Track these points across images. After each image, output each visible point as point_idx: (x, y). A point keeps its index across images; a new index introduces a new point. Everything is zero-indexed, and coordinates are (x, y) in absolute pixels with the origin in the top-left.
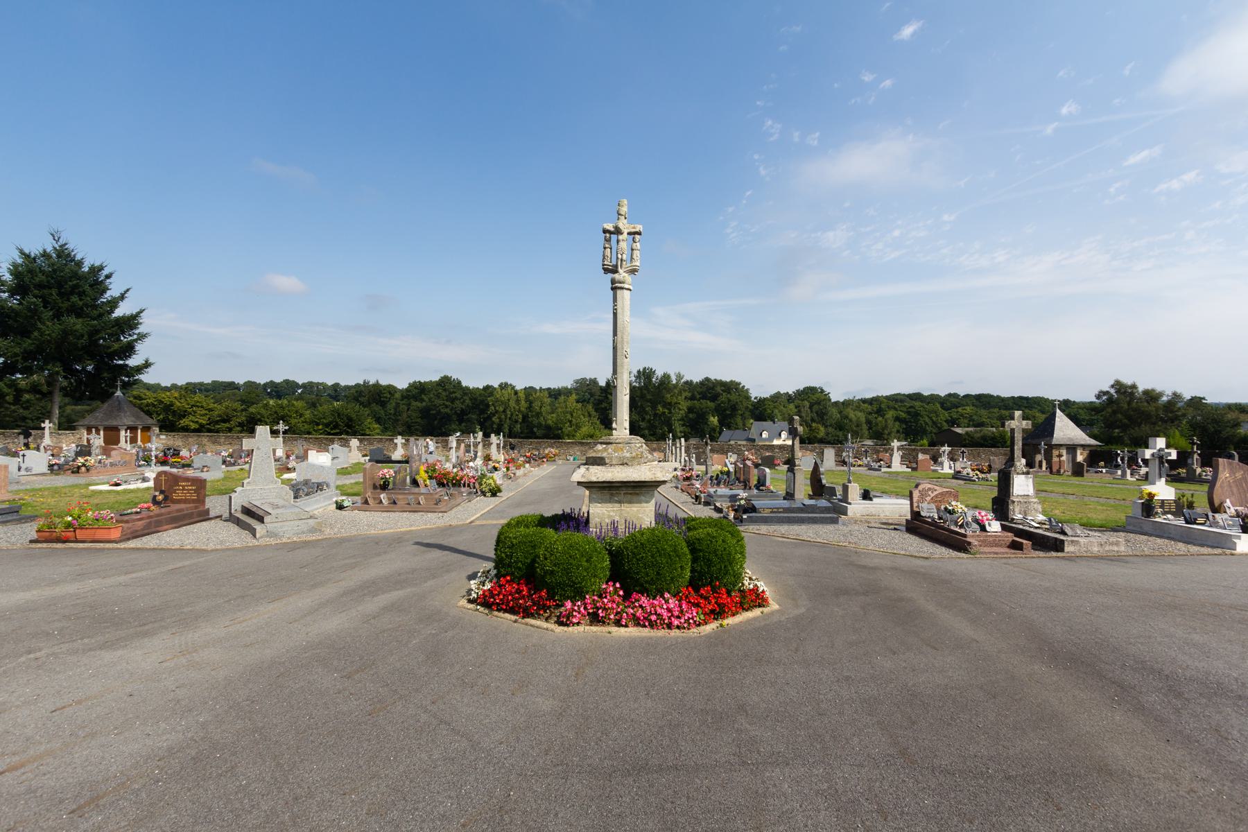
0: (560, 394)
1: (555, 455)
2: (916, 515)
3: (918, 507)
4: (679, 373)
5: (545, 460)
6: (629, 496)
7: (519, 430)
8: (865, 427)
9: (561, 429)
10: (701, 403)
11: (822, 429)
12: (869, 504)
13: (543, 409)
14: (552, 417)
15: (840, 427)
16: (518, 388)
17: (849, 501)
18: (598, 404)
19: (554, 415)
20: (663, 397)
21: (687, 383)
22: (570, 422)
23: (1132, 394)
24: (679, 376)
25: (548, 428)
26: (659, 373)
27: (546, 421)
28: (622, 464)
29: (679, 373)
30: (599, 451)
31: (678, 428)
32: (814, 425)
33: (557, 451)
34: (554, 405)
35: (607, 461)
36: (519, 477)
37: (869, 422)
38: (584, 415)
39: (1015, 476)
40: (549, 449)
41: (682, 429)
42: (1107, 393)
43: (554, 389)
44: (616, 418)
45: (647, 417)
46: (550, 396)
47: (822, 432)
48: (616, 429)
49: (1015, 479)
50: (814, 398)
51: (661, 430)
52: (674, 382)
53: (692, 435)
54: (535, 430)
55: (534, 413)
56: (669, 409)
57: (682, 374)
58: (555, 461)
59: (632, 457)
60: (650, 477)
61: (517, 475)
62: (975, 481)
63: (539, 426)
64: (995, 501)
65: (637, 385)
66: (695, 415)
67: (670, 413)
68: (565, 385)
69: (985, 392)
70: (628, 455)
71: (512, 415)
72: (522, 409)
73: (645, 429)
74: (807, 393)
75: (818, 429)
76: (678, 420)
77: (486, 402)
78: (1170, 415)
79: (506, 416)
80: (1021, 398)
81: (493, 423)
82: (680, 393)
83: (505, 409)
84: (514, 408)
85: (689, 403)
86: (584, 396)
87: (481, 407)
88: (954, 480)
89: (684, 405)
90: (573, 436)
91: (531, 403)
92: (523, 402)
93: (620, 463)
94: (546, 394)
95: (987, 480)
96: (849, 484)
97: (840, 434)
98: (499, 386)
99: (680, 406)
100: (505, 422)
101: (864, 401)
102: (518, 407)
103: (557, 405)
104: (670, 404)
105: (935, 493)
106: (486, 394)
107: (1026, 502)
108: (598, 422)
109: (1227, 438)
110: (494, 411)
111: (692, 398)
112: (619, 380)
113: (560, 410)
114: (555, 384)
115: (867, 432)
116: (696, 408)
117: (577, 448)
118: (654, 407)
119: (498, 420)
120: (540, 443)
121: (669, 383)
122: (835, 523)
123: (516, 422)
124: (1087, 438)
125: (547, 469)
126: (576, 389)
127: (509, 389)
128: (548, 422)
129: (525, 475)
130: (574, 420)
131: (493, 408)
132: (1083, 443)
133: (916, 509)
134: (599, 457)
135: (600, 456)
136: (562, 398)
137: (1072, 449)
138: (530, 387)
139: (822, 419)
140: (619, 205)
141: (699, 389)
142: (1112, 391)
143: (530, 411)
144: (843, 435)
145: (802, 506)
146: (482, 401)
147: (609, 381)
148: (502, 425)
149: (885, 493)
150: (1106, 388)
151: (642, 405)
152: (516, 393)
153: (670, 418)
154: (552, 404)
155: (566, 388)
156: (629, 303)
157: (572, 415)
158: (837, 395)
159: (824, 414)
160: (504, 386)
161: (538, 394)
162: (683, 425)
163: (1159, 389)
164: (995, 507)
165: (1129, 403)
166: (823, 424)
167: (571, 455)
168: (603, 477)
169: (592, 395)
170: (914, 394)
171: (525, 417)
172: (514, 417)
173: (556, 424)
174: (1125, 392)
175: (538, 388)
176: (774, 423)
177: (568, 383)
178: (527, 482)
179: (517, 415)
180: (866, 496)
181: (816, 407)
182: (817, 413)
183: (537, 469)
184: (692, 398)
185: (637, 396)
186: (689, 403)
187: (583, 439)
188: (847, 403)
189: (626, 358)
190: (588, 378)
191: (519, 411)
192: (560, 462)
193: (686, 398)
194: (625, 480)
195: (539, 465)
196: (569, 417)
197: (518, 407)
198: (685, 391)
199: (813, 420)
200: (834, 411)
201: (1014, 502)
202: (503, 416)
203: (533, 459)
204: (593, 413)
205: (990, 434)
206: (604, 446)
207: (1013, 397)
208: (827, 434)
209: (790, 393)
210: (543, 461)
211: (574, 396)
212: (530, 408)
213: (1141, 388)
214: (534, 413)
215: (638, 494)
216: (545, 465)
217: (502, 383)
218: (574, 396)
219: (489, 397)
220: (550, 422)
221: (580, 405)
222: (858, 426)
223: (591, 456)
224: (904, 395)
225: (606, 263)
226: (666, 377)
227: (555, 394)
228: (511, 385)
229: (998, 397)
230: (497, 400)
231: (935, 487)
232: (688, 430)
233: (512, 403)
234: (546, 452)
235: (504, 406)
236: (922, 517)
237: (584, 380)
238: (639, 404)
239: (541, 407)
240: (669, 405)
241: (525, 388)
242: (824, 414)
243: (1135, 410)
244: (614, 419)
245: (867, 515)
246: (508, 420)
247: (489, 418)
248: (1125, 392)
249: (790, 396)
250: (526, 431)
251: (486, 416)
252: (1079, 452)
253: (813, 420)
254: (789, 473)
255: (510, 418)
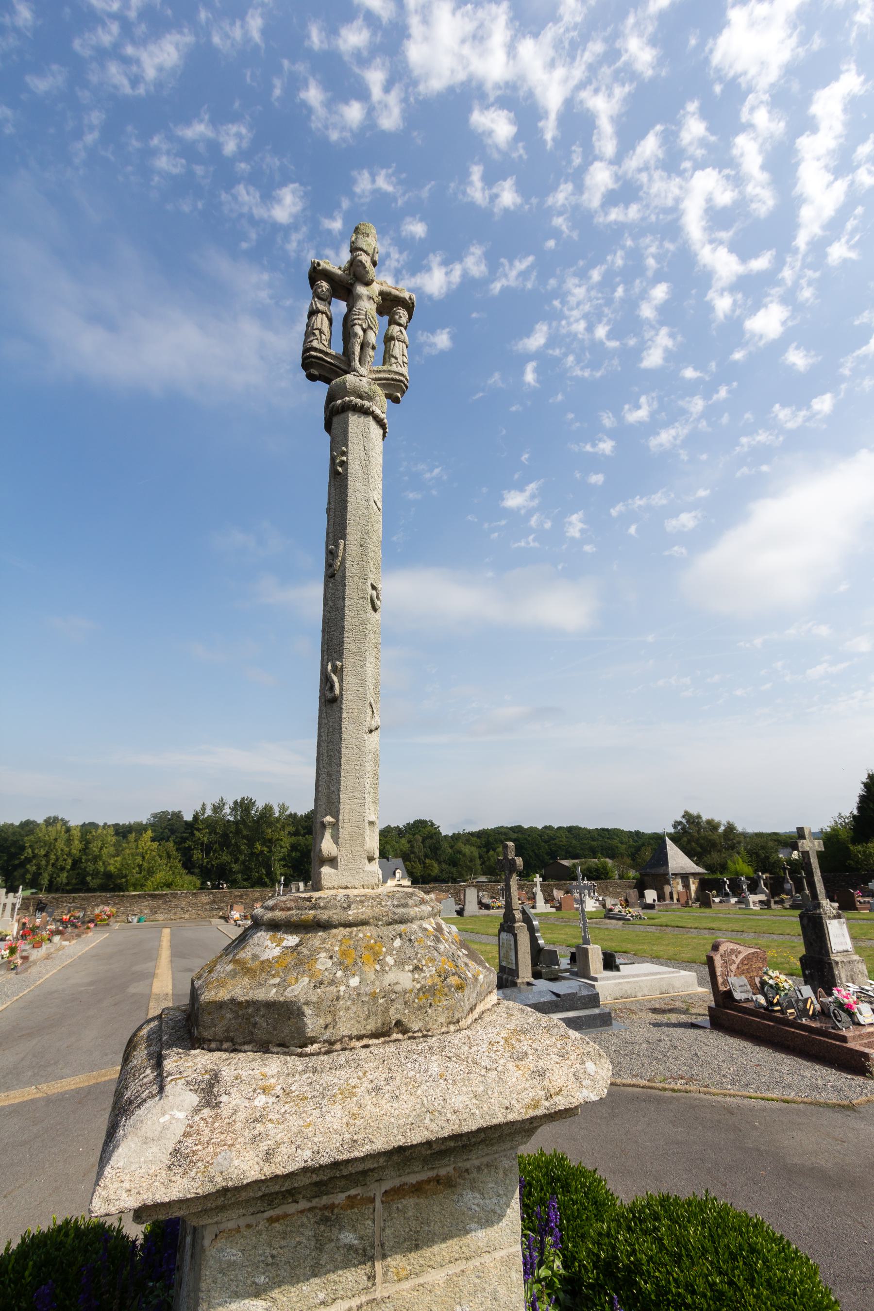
0: (130, 832)
1: (109, 916)
2: (724, 999)
3: (725, 982)
4: (283, 805)
5: (92, 925)
6: (409, 1202)
7: (65, 881)
8: (478, 862)
9: (126, 876)
10: (306, 839)
11: (436, 865)
12: (614, 978)
13: (105, 851)
14: (116, 861)
15: (453, 863)
16: (72, 824)
17: (592, 974)
18: (180, 843)
19: (118, 859)
20: (263, 832)
21: (290, 815)
22: (140, 866)
23: (699, 823)
24: (283, 808)
25: (108, 876)
26: (260, 804)
27: (106, 868)
28: (380, 1034)
29: (283, 805)
30: (267, 966)
31: (278, 868)
32: (427, 861)
33: (114, 910)
34: (120, 846)
35: (313, 1023)
36: (35, 963)
37: (481, 857)
38: (161, 857)
39: (828, 922)
40: (101, 907)
41: (283, 871)
42: (680, 823)
43: (124, 825)
44: (336, 815)
45: (242, 858)
46: (117, 833)
47: (436, 869)
48: (332, 861)
49: (829, 926)
50: (425, 831)
51: (258, 872)
52: (277, 814)
53: (294, 877)
54: (89, 879)
55: (90, 857)
56: (269, 847)
57: (287, 805)
58: (108, 924)
59: (423, 990)
60: (528, 1097)
61: (32, 959)
62: (629, 920)
63: (95, 874)
64: (805, 961)
65: (232, 819)
66: (298, 854)
67: (270, 851)
68: (138, 820)
69: (575, 825)
70: (405, 979)
71: (57, 859)
72: (74, 851)
73: (238, 872)
74: (417, 827)
75: (432, 866)
76: (280, 860)
77: (21, 843)
78: (730, 843)
79: (48, 862)
80: (603, 830)
81: (27, 871)
82: (283, 827)
83: (48, 852)
84: (62, 850)
85: (293, 839)
86: (162, 833)
87: (12, 850)
88: (608, 921)
89: (287, 842)
90: (142, 886)
91: (88, 842)
92: (76, 842)
93: (371, 1026)
94: (111, 831)
95: (640, 918)
96: (588, 947)
97: (454, 870)
98: (45, 821)
99: (282, 843)
100: (46, 869)
101: (472, 834)
102: (68, 849)
103: (124, 845)
104: (270, 840)
105: (741, 957)
106: (23, 833)
107: (849, 962)
108: (180, 865)
109: (775, 863)
110: (31, 855)
111: (296, 834)
112: (350, 679)
113: (128, 851)
114: (125, 820)
115: (479, 867)
116: (300, 845)
117: (146, 904)
118: (251, 845)
119: (34, 868)
120: (87, 899)
121: (270, 815)
122: (608, 1025)
123: (62, 869)
124: (696, 866)
125: (94, 939)
126: (152, 825)
127: (59, 825)
128: (108, 868)
129: (48, 957)
130: (145, 864)
131: (30, 851)
132: (693, 871)
133: (722, 988)
134: (270, 1005)
135: (272, 994)
136: (132, 836)
137: (685, 877)
138: (90, 823)
139: (436, 854)
140: (357, 230)
141: (303, 824)
142: (684, 821)
143: (86, 854)
144: (457, 871)
145: (554, 998)
146: (15, 843)
147: (197, 813)
148: (41, 874)
149: (638, 957)
150: (679, 819)
151: (236, 843)
152: (68, 830)
153: (269, 858)
154: (117, 845)
155: (140, 825)
156: (380, 460)
157: (143, 858)
158: (446, 830)
159: (437, 849)
160: (51, 822)
161: (100, 831)
162: (284, 866)
163: (716, 819)
164: (807, 972)
165: (698, 832)
166: (437, 860)
167: (135, 915)
168: (297, 1140)
169: (173, 832)
170: (516, 827)
171: (76, 863)
172: (61, 863)
173: (119, 870)
174: (694, 822)
175: (101, 824)
176: (388, 860)
177: (144, 818)
178: (47, 972)
179: (65, 860)
180: (610, 963)
181: (429, 842)
182: (430, 848)
183: (74, 942)
184: (296, 834)
185: (231, 832)
186: (293, 839)
187: (157, 889)
188: (456, 837)
189: (375, 609)
190: (170, 811)
191: (69, 854)
192: (117, 926)
193: (289, 833)
194: (416, 1138)
195: (79, 936)
196: (139, 860)
197: (68, 849)
198: (289, 825)
199: (426, 856)
200: (446, 845)
201: (837, 963)
202: (44, 863)
203: (72, 926)
204: (174, 853)
205: (594, 865)
206: (292, 940)
207: (597, 829)
208: (442, 871)
209: (401, 826)
210: (88, 928)
211: (150, 833)
212: (85, 850)
213: (705, 818)
214: (90, 857)
215: (449, 1183)
216: (90, 934)
217: (49, 818)
218: (150, 833)
219: (27, 835)
220: (112, 868)
221: (155, 845)
222: (471, 861)
223: (223, 995)
224: (507, 828)
225: (315, 344)
226: (268, 809)
227: (123, 832)
228: (62, 820)
229: (585, 829)
230: (39, 840)
231: (738, 946)
232: (289, 871)
233: (61, 845)
234: (97, 911)
235: (47, 848)
236: (736, 1001)
237: (165, 813)
238: (233, 841)
239: (101, 848)
240: (269, 842)
241: (84, 825)
242: (437, 849)
243: (704, 838)
244: (329, 819)
245: (622, 997)
246: (50, 867)
247: (22, 864)
248: (694, 822)
249: (400, 830)
250: (74, 881)
251: (17, 862)
252: (691, 880)
253: (426, 856)
254: (504, 935)
255: (53, 865)
